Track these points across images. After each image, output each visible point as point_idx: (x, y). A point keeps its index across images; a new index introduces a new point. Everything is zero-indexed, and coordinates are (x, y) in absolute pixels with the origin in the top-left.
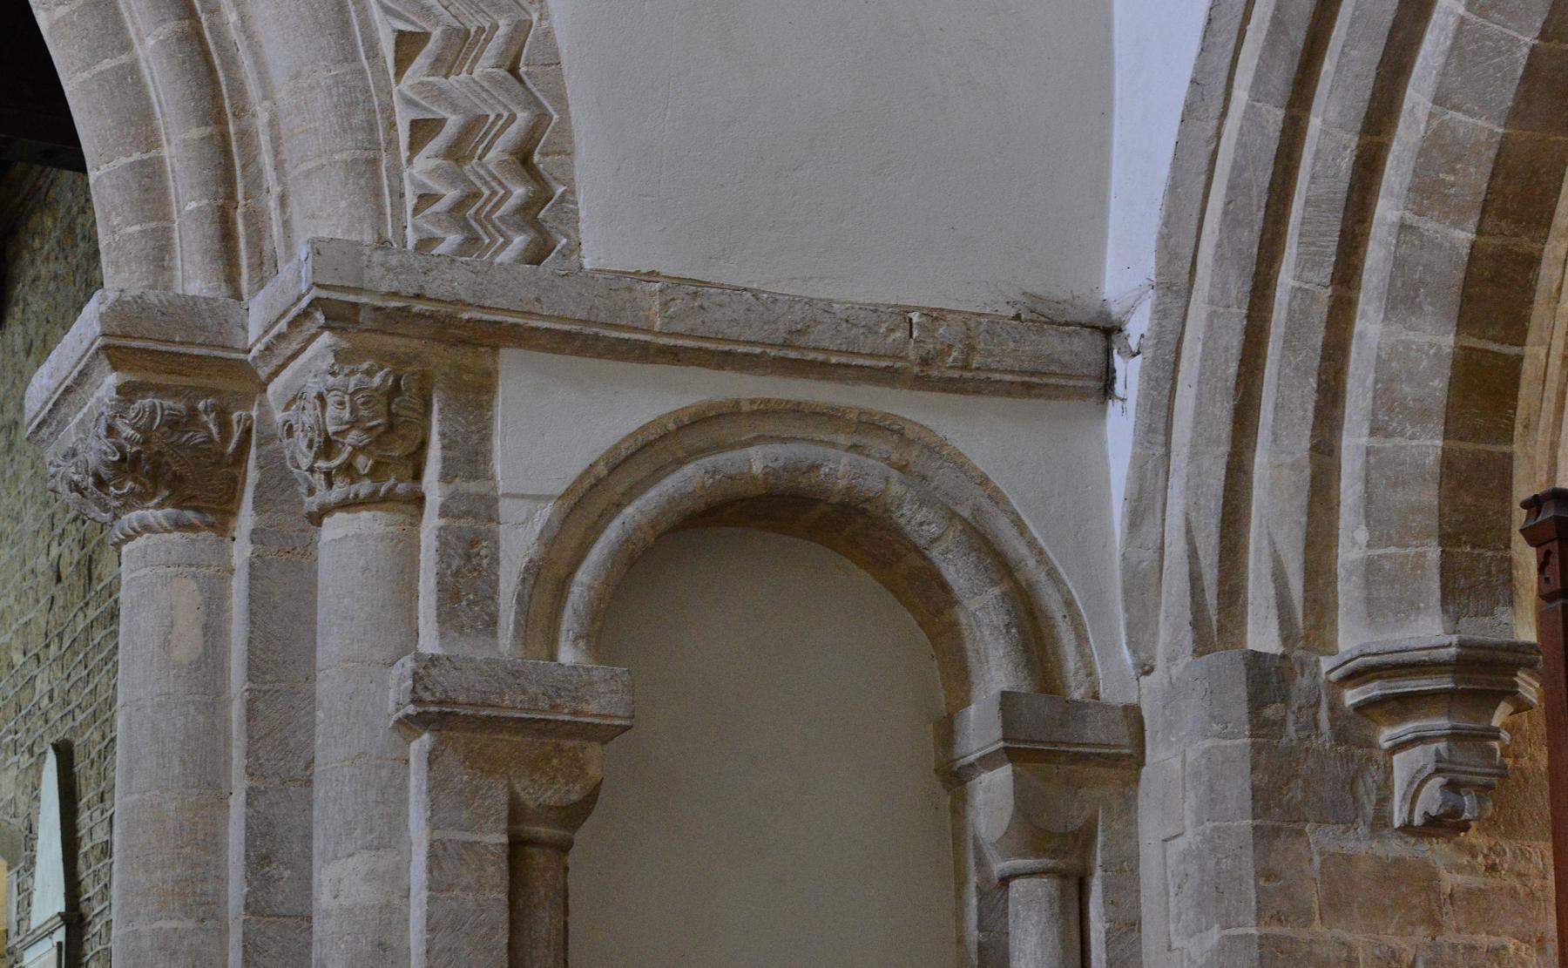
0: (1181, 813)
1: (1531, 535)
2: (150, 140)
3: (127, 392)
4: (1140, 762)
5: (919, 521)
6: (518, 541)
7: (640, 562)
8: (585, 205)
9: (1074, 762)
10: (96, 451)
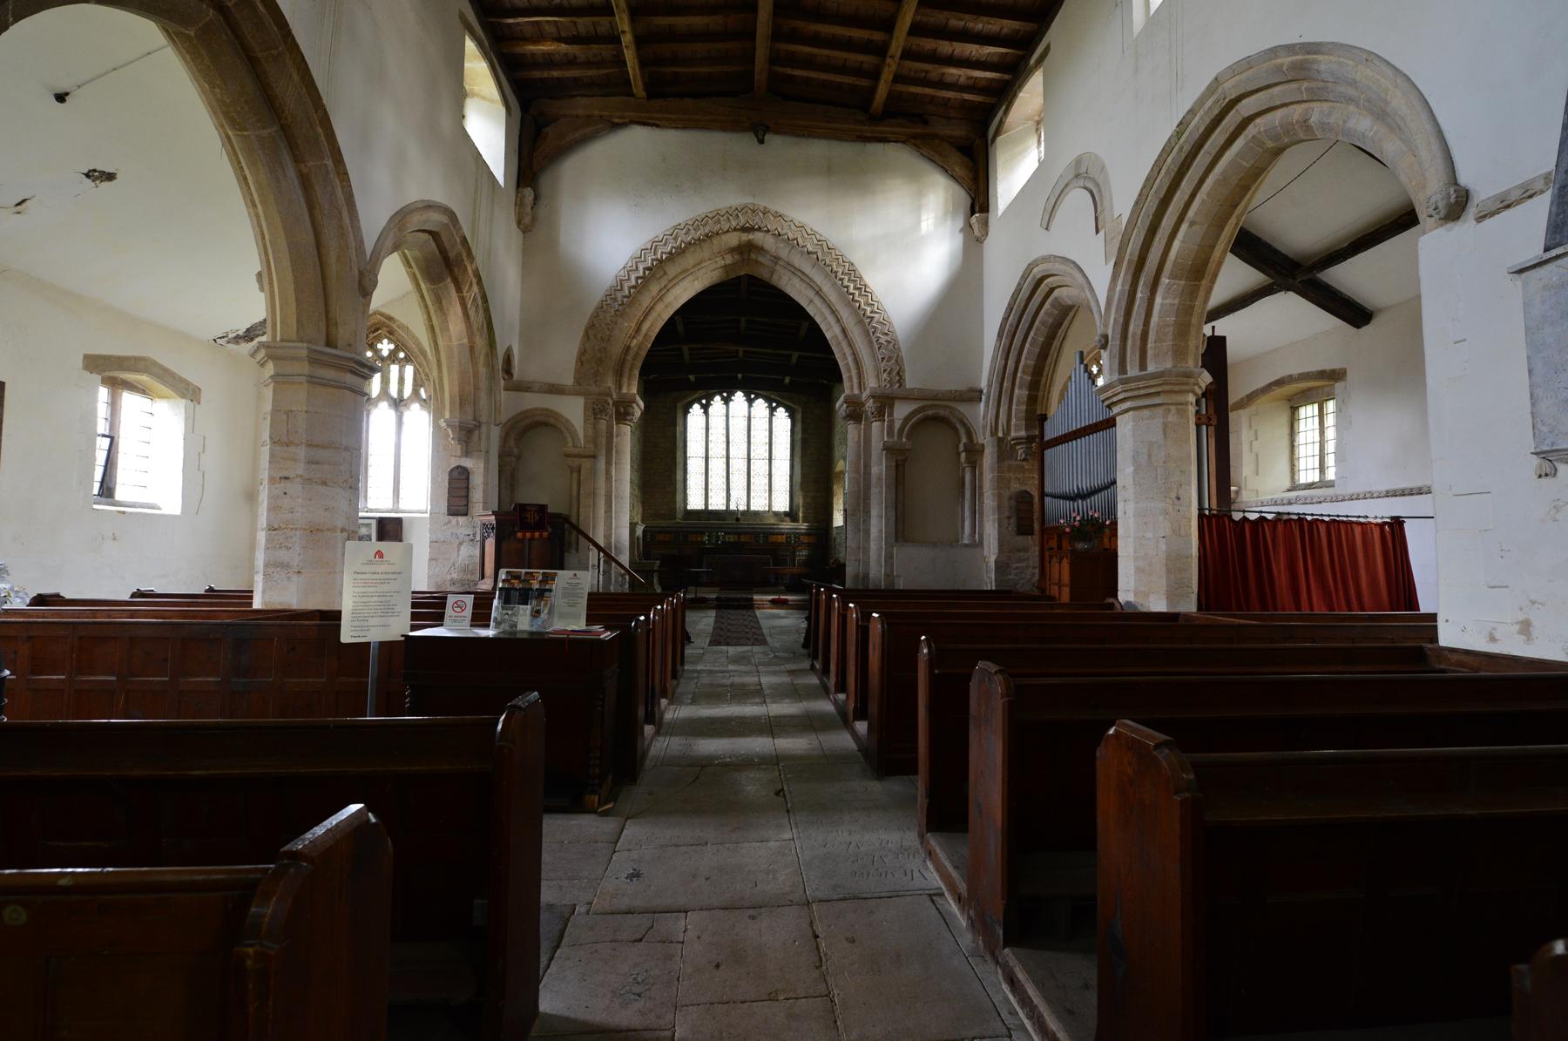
0: (988, 459)
6: (897, 425)
7: (913, 427)
9: (975, 452)
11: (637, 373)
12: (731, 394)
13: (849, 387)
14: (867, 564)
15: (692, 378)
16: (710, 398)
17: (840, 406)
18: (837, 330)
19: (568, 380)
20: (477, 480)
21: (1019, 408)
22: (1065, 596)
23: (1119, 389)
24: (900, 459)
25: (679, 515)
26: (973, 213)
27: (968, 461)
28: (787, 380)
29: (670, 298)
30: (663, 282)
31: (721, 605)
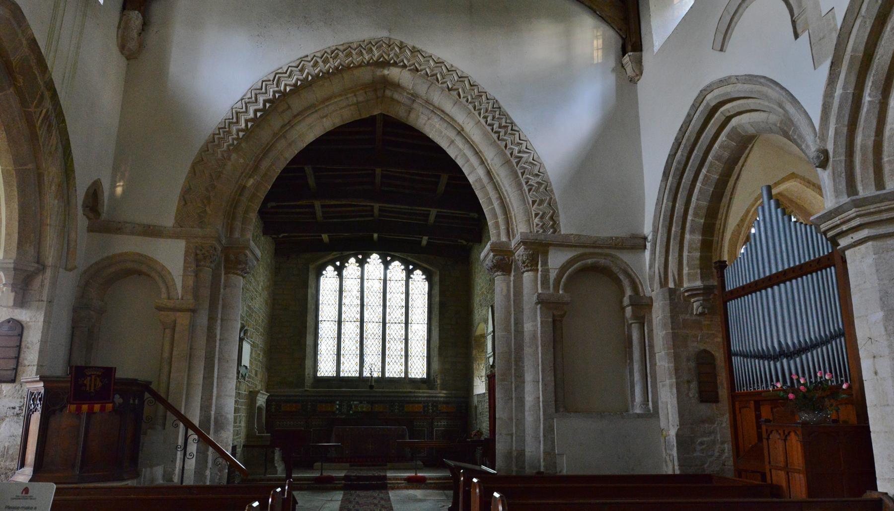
0: (659, 314)
1: (716, 268)
2: (497, 218)
3: (494, 256)
4: (652, 305)
5: (615, 269)
6: (553, 275)
7: (570, 277)
8: (561, 225)
9: (642, 306)
10: (490, 264)
11: (253, 216)
12: (367, 256)
13: (496, 233)
14: (522, 439)
15: (325, 237)
16: (344, 260)
17: (485, 254)
18: (481, 172)
19: (169, 222)
20: (33, 338)
21: (691, 255)
22: (799, 488)
23: (852, 212)
24: (556, 313)
25: (309, 381)
26: (624, 55)
27: (635, 316)
28: (425, 241)
29: (294, 134)
30: (287, 116)
31: (350, 485)
